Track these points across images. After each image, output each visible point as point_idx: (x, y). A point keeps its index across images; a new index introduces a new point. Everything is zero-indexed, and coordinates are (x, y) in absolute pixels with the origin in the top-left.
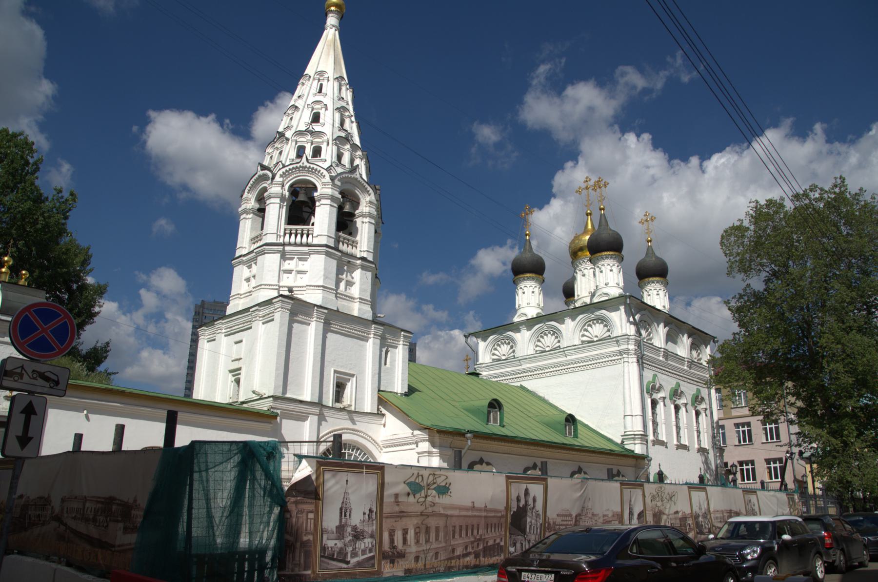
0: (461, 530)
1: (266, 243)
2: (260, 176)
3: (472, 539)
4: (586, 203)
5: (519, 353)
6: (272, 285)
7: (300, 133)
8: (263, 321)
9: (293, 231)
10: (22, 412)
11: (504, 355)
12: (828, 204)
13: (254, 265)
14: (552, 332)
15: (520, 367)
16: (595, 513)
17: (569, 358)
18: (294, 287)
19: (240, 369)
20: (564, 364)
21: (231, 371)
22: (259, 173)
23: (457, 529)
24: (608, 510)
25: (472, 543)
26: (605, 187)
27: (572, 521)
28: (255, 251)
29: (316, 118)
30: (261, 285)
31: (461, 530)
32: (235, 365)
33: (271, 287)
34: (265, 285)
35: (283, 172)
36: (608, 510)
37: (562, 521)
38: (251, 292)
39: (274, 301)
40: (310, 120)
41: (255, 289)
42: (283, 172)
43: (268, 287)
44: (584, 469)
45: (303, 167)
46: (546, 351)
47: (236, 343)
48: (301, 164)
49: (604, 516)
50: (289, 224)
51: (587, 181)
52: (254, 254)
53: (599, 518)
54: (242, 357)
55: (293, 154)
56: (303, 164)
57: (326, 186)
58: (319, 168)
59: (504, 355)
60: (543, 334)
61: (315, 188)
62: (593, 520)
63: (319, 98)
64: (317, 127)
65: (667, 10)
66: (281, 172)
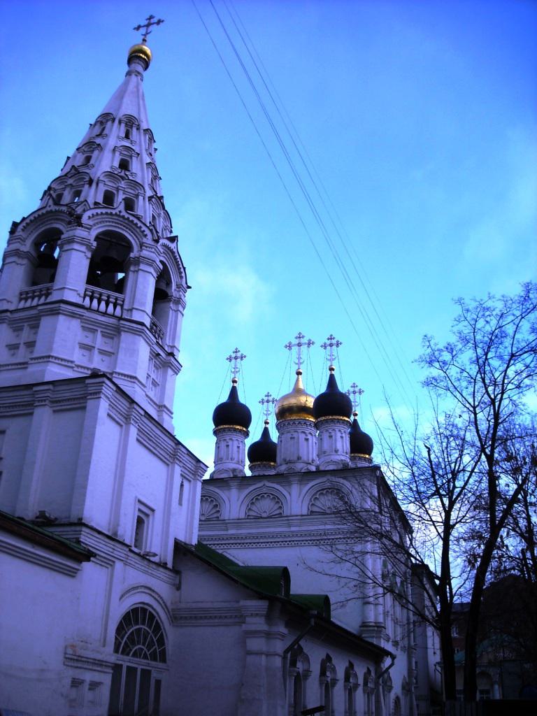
4: (233, 370)
5: (226, 515)
8: (55, 409)
9: (104, 298)
13: (26, 329)
14: (272, 497)
15: (225, 533)
17: (293, 529)
20: (225, 537)
22: (48, 209)
28: (40, 308)
29: (124, 165)
33: (63, 363)
35: (24, 227)
38: (26, 363)
41: (33, 361)
42: (24, 227)
45: (119, 216)
46: (261, 518)
56: (120, 212)
59: (265, 512)
60: (259, 497)
61: (129, 247)
63: (126, 143)
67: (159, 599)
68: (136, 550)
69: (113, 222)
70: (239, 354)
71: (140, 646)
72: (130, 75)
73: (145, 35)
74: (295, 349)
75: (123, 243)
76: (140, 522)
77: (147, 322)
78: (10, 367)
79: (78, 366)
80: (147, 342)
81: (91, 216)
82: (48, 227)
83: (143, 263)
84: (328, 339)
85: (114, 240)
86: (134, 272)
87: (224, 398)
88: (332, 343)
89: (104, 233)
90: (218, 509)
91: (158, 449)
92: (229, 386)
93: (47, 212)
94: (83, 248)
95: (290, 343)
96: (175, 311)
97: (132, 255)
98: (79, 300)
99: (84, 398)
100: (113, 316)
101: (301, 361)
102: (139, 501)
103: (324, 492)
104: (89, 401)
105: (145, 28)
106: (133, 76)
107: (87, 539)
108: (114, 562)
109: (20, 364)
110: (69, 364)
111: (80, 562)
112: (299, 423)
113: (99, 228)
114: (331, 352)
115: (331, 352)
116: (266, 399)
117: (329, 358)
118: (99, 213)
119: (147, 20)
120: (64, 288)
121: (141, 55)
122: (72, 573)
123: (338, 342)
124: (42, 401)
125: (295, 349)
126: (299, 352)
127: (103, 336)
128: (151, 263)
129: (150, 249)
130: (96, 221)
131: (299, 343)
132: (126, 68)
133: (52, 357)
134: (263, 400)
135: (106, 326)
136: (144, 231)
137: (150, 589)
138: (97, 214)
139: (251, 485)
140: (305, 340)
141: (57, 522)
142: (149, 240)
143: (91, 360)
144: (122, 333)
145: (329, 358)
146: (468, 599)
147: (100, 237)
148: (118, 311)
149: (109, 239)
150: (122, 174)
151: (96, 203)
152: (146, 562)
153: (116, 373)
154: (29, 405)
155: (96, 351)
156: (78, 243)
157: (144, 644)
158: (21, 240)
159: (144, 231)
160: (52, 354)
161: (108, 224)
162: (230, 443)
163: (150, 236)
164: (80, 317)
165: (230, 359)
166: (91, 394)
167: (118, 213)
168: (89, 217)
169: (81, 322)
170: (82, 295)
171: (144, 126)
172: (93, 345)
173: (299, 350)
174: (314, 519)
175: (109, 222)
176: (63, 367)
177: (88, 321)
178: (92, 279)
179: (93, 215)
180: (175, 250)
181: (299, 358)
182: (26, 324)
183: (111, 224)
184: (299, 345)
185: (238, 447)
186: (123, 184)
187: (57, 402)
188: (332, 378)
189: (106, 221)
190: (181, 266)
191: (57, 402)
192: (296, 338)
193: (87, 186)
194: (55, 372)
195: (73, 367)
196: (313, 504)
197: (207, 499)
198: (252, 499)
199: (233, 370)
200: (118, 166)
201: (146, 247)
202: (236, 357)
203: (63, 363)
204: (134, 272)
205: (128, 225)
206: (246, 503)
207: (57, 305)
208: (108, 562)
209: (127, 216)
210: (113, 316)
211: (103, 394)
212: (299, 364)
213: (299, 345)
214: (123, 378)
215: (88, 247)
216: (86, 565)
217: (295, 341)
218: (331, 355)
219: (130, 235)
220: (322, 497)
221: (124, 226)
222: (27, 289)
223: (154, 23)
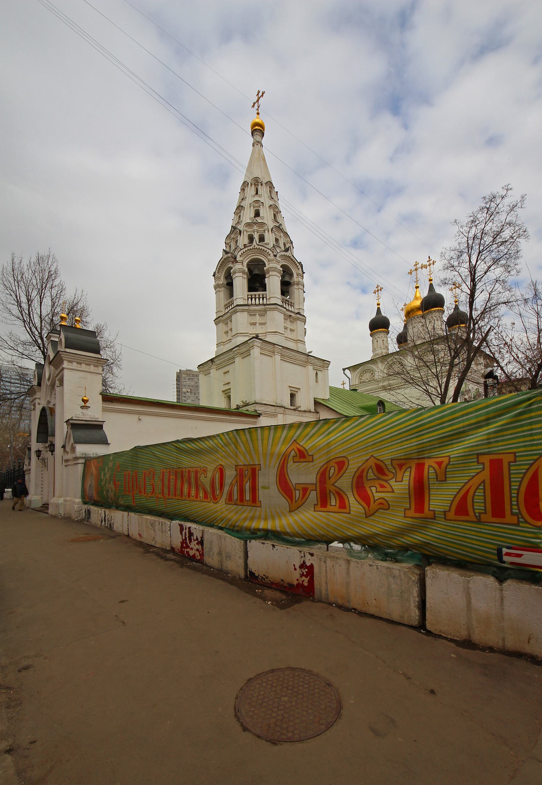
1: (237, 305)
2: (225, 259)
4: (377, 298)
5: (376, 377)
6: (244, 333)
7: (248, 225)
8: (242, 357)
10: (62, 448)
11: (367, 379)
13: (229, 322)
19: (230, 389)
21: (223, 391)
22: (224, 257)
26: (433, 265)
28: (230, 311)
29: (257, 214)
30: (237, 334)
32: (227, 387)
34: (240, 333)
37: (520, 556)
38: (231, 339)
39: (249, 342)
40: (254, 216)
45: (254, 249)
47: (225, 373)
48: (253, 246)
50: (249, 291)
52: (229, 314)
54: (230, 381)
55: (246, 241)
56: (254, 246)
58: (265, 249)
59: (367, 379)
61: (264, 265)
63: (257, 198)
64: (259, 220)
66: (240, 254)
68: (292, 408)
69: (253, 253)
70: (379, 288)
73: (258, 109)
75: (261, 263)
76: (292, 396)
78: (227, 342)
80: (280, 312)
81: (241, 254)
82: (227, 267)
83: (270, 271)
85: (256, 263)
86: (268, 277)
87: (373, 315)
89: (251, 261)
91: (297, 361)
92: (377, 307)
94: (241, 274)
96: (298, 289)
97: (265, 268)
100: (263, 304)
102: (289, 386)
104: (251, 351)
109: (229, 340)
110: (246, 335)
113: (247, 259)
118: (247, 250)
124: (237, 355)
126: (417, 274)
128: (274, 270)
129: (273, 262)
130: (245, 256)
132: (251, 140)
135: (260, 311)
136: (268, 252)
138: (246, 251)
141: (250, 404)
142: (272, 257)
147: (249, 264)
149: (254, 263)
151: (245, 245)
152: (297, 411)
154: (233, 358)
156: (238, 272)
158: (218, 278)
161: (250, 256)
162: (378, 339)
163: (272, 254)
164: (246, 310)
167: (254, 247)
168: (240, 255)
169: (248, 312)
170: (247, 299)
171: (265, 181)
172: (256, 322)
173: (416, 273)
174: (372, 382)
175: (251, 254)
176: (244, 337)
178: (251, 288)
179: (242, 253)
180: (290, 255)
182: (228, 321)
183: (252, 255)
187: (242, 354)
188: (379, 309)
189: (248, 255)
190: (296, 263)
191: (242, 354)
193: (239, 236)
195: (248, 336)
196: (360, 379)
197: (368, 371)
199: (377, 298)
204: (268, 277)
205: (260, 252)
206: (358, 375)
207: (235, 308)
210: (263, 304)
211: (255, 346)
212: (417, 282)
214: (271, 333)
215: (243, 272)
219: (263, 257)
221: (259, 254)
222: (226, 303)
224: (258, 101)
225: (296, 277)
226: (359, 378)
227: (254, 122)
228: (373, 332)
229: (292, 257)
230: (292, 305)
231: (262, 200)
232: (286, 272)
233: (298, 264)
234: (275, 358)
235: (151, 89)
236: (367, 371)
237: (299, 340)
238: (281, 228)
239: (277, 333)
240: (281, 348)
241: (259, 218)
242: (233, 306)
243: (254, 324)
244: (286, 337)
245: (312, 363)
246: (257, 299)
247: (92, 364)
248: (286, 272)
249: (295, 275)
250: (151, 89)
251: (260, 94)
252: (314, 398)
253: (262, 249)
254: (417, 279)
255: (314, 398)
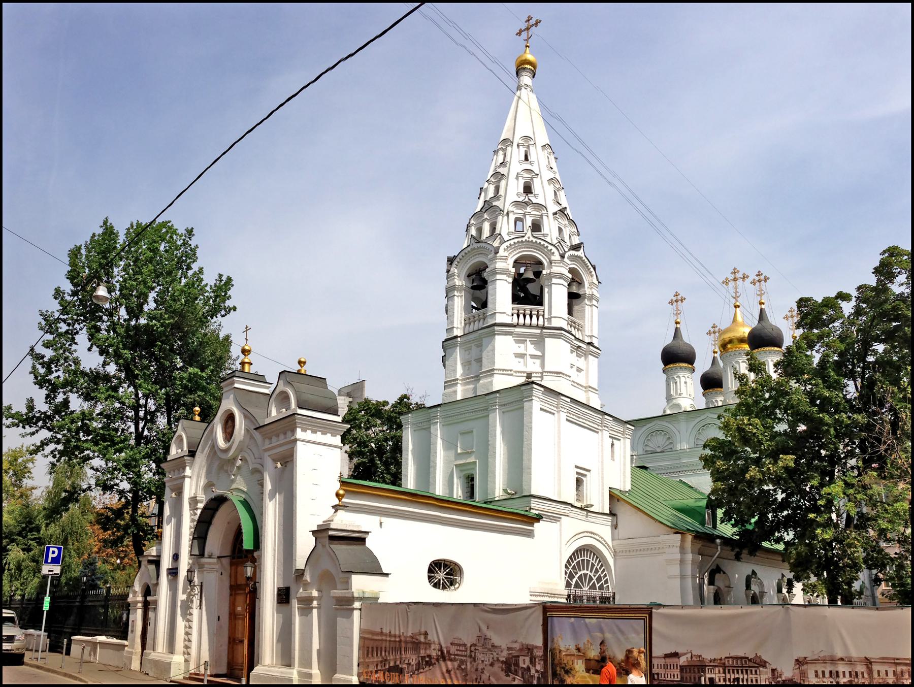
0: (373, 651)
3: (380, 659)
6: (506, 370)
7: (517, 204)
12: (800, 314)
15: (678, 462)
16: (496, 645)
18: (534, 373)
22: (471, 247)
23: (370, 650)
24: (516, 642)
25: (381, 662)
27: (466, 651)
29: (528, 189)
31: (373, 651)
33: (505, 372)
36: (516, 642)
37: (457, 650)
43: (501, 372)
44: (759, 575)
45: (528, 241)
48: (526, 238)
49: (509, 649)
51: (735, 273)
53: (502, 651)
56: (529, 238)
57: (557, 264)
62: (495, 654)
63: (527, 166)
65: (486, 53)
67: (600, 539)
68: (578, 505)
70: (679, 298)
71: (585, 572)
72: (520, 90)
74: (731, 284)
76: (579, 482)
77: (564, 325)
79: (516, 372)
80: (566, 341)
84: (757, 276)
87: (668, 340)
88: (761, 279)
90: (671, 441)
92: (674, 326)
93: (472, 250)
95: (727, 278)
98: (508, 320)
99: (521, 401)
100: (537, 327)
101: (738, 295)
102: (577, 467)
103: (654, 434)
105: (526, 32)
106: (523, 89)
107: (536, 507)
108: (560, 518)
110: (509, 372)
111: (532, 524)
112: (740, 354)
114: (760, 288)
115: (760, 288)
116: (712, 330)
117: (759, 293)
119: (526, 22)
120: (495, 313)
121: (526, 66)
122: (530, 534)
123: (765, 277)
125: (731, 284)
127: (532, 344)
128: (560, 276)
131: (735, 278)
133: (496, 370)
134: (710, 331)
136: (551, 250)
137: (591, 533)
139: (696, 418)
140: (740, 275)
142: (556, 257)
143: (525, 365)
144: (546, 339)
145: (759, 293)
146: (744, 551)
148: (541, 322)
150: (527, 200)
153: (545, 372)
155: (528, 357)
157: (587, 570)
159: (551, 250)
160: (495, 368)
162: (678, 380)
163: (557, 253)
165: (671, 303)
166: (526, 397)
173: (735, 284)
177: (519, 335)
178: (516, 299)
180: (583, 255)
181: (736, 292)
184: (735, 280)
185: (686, 383)
186: (529, 209)
188: (762, 312)
192: (732, 273)
194: (500, 382)
197: (657, 433)
198: (699, 430)
200: (522, 192)
201: (555, 263)
202: (677, 299)
203: (505, 372)
206: (642, 439)
208: (555, 518)
209: (534, 240)
210: (537, 327)
213: (677, 301)
216: (536, 525)
217: (731, 277)
218: (761, 290)
220: (704, 431)
223: (532, 26)
224: (527, 29)
225: (588, 288)
226: (644, 443)
227: (521, 59)
228: (669, 366)
229: (584, 258)
230: (579, 328)
231: (535, 169)
232: (575, 279)
233: (592, 269)
234: (602, 434)
235: (439, 26)
236: (658, 433)
237: (590, 387)
238: (566, 213)
239: (561, 375)
240: (568, 400)
241: (532, 195)
242: (481, 325)
243: (522, 356)
244: (573, 381)
245: (608, 427)
246: (528, 317)
247: (319, 431)
248: (575, 279)
249: (587, 285)
250: (439, 26)
251: (532, 22)
252: (610, 488)
253: (540, 243)
254: (736, 294)
255: (610, 488)
